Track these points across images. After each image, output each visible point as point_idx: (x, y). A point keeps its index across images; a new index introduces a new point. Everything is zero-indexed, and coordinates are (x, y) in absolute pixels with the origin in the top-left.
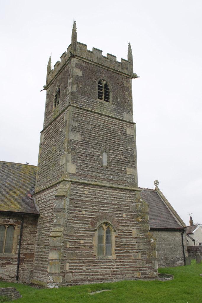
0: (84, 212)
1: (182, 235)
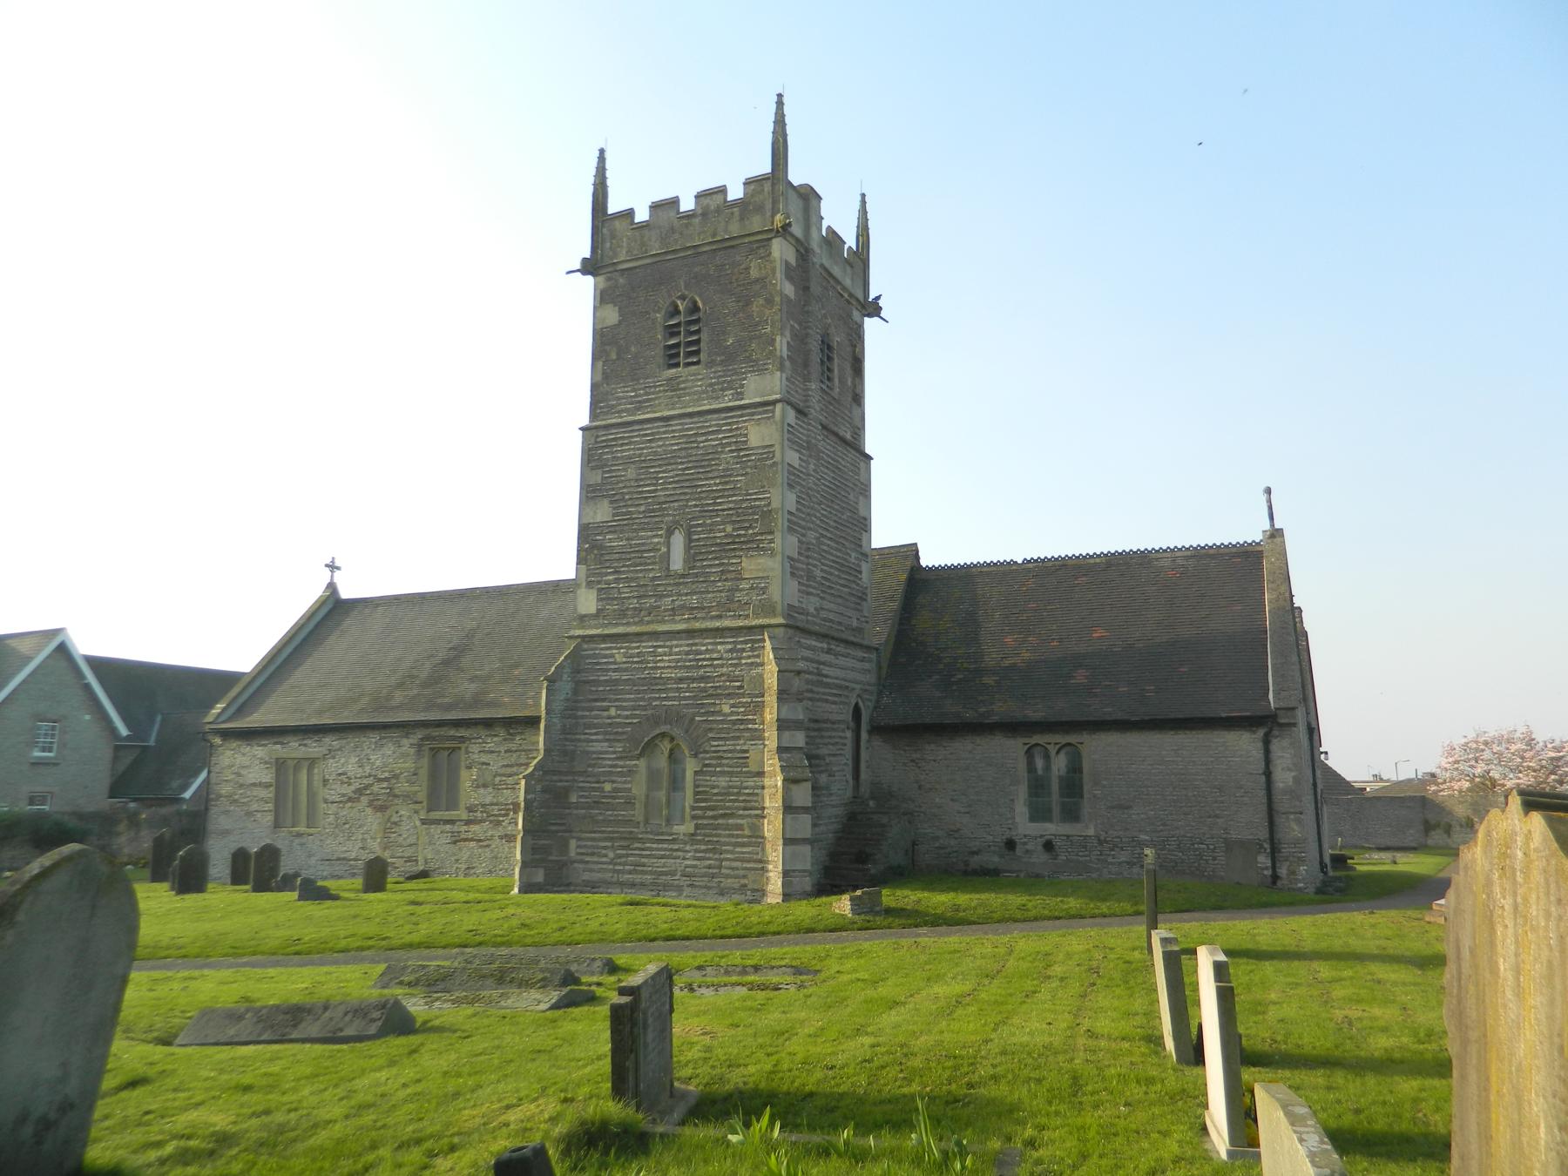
0: (613, 712)
1: (1267, 742)
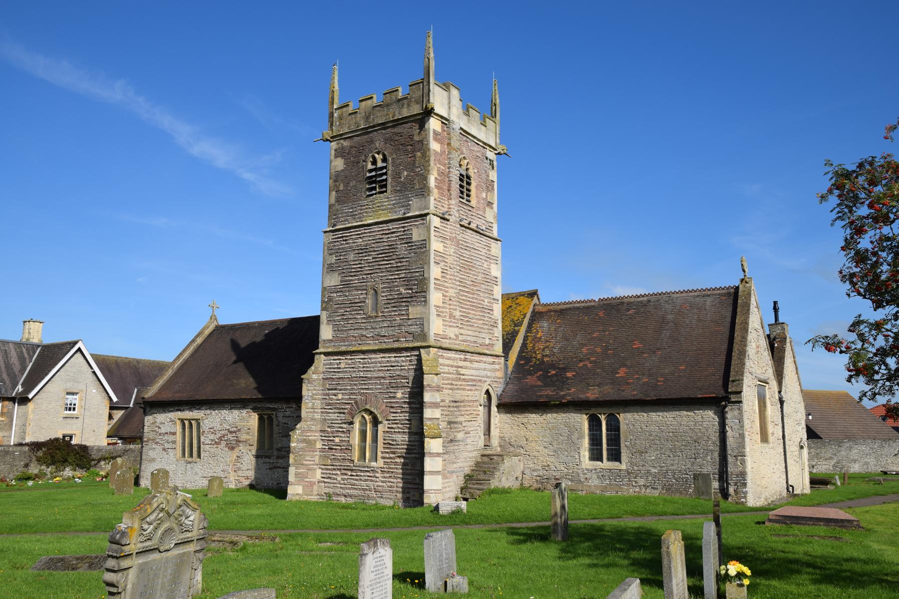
0: (340, 396)
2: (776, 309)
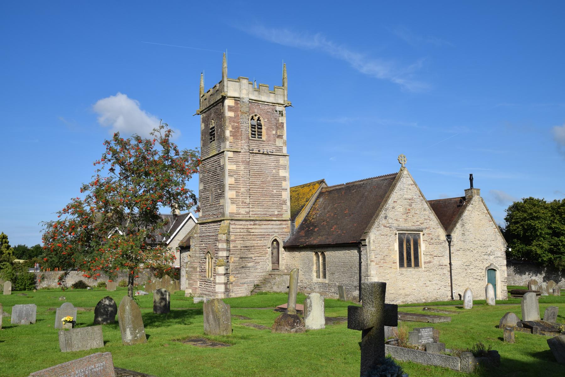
2: (471, 179)
